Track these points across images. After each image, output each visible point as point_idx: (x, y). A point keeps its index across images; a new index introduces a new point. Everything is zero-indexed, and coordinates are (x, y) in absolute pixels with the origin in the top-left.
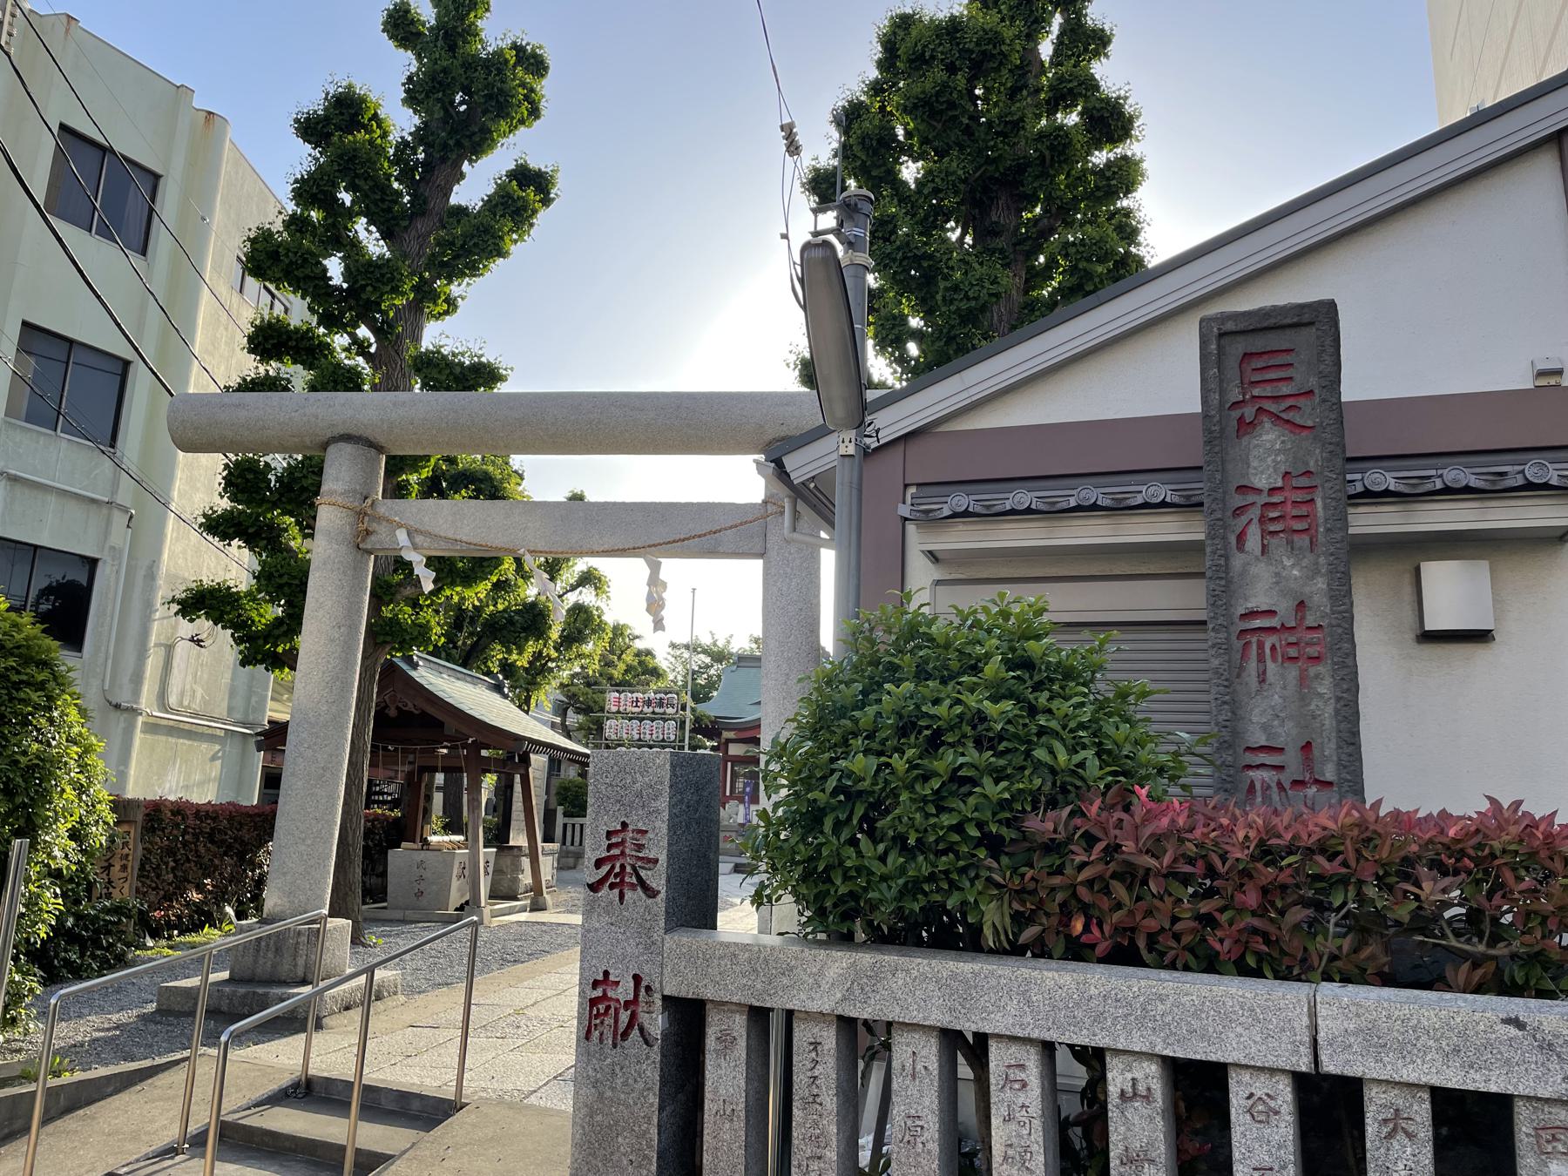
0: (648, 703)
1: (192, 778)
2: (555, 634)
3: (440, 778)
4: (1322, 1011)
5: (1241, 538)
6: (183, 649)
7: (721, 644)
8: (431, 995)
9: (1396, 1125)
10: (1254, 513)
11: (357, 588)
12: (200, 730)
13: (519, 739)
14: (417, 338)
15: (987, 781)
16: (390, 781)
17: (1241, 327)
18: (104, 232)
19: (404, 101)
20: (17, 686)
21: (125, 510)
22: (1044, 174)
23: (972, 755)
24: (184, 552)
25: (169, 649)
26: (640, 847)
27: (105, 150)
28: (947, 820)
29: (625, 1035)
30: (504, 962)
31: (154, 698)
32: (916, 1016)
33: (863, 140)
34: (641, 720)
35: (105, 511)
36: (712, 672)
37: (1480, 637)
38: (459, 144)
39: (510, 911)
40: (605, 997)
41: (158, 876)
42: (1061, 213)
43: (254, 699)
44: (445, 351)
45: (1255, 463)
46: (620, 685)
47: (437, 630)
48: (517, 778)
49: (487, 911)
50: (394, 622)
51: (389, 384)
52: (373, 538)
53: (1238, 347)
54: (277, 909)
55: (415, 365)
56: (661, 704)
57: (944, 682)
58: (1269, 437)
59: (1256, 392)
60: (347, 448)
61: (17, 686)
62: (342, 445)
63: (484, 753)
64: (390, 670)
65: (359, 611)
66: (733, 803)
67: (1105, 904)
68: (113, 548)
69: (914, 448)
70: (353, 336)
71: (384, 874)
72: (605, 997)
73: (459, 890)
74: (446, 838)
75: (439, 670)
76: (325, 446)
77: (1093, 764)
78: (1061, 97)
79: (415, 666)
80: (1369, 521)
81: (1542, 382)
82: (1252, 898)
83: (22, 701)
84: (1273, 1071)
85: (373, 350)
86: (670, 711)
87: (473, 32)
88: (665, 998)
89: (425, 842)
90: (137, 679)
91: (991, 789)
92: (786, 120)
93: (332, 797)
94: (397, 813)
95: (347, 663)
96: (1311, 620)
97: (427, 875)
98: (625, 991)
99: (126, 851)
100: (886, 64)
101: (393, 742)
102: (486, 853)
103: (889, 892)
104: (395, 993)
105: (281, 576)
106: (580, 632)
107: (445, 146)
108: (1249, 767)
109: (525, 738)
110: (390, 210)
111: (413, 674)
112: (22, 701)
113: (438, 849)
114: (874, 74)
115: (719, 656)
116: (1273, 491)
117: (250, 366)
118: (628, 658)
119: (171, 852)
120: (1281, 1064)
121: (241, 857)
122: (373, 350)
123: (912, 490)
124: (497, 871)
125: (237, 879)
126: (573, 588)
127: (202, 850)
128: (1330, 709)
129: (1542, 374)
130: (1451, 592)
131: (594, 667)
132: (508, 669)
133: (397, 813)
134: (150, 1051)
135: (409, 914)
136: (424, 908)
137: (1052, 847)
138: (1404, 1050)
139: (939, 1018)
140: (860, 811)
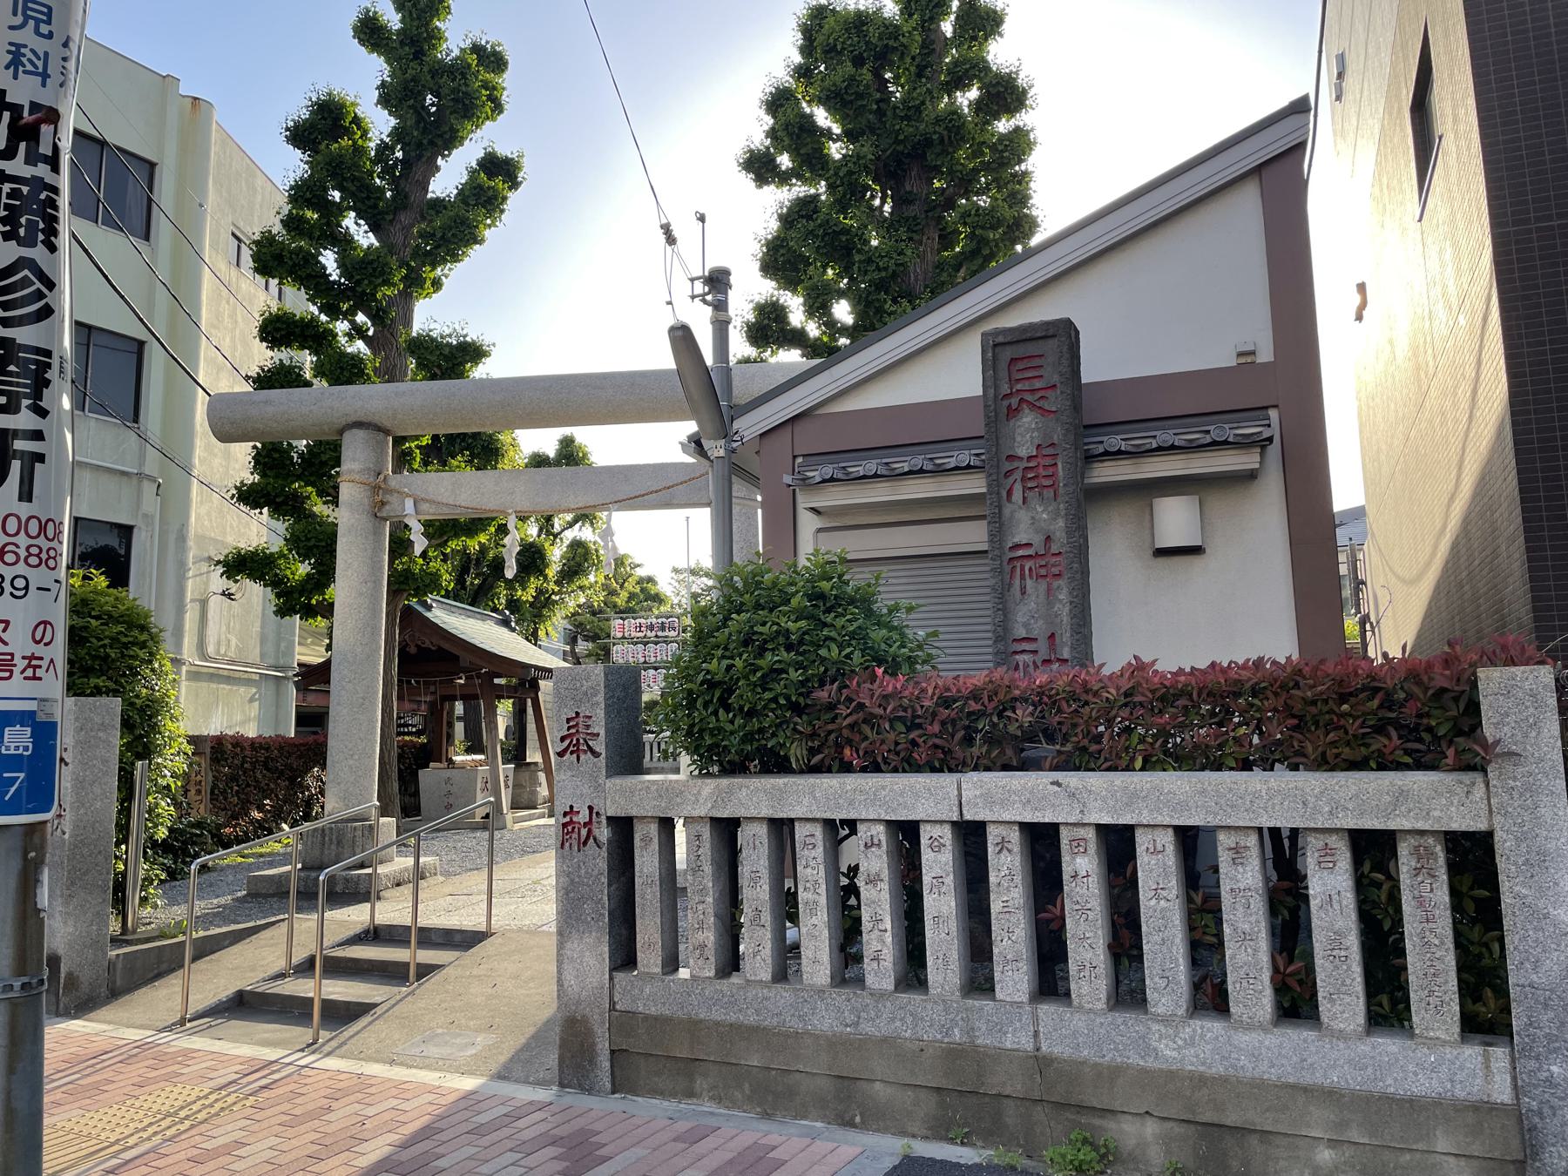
0: (651, 627)
1: (241, 716)
2: (552, 572)
3: (459, 708)
4: (964, 786)
5: (1010, 493)
6: (216, 602)
8: (465, 876)
9: (1002, 845)
10: (1018, 475)
11: (379, 549)
12: (237, 675)
13: (527, 667)
14: (408, 322)
15: (791, 670)
16: (414, 713)
17: (1008, 339)
18: (110, 223)
19: (379, 102)
20: (126, 646)
21: (153, 480)
22: (945, 152)
23: (784, 655)
24: (209, 514)
25: (204, 603)
26: (588, 727)
27: (102, 143)
28: (768, 695)
29: (585, 843)
30: (524, 853)
32: (753, 813)
33: (787, 126)
35: (135, 481)
37: (1195, 551)
38: (432, 143)
39: (530, 818)
40: (572, 821)
42: (966, 184)
43: (283, 645)
44: (434, 334)
45: (1018, 439)
47: (446, 576)
51: (390, 374)
53: (1007, 354)
55: (409, 347)
56: (663, 629)
57: (771, 611)
58: (1028, 419)
59: (1019, 387)
60: (360, 434)
61: (126, 646)
62: (355, 431)
63: (496, 681)
64: (408, 611)
65: (382, 567)
67: (857, 738)
68: (145, 516)
69: (799, 427)
70: (353, 323)
72: (572, 821)
74: (469, 758)
75: (450, 610)
76: (341, 432)
77: (857, 657)
78: (958, 81)
79: (429, 608)
80: (1107, 473)
81: (1242, 360)
82: (936, 728)
83: (131, 657)
84: (942, 822)
85: (370, 333)
86: (672, 633)
87: (435, 36)
88: (609, 818)
89: (450, 761)
91: (795, 675)
92: (664, 221)
93: (372, 721)
94: (423, 739)
95: (375, 612)
96: (1054, 549)
97: (454, 789)
98: (583, 817)
100: (807, 49)
101: (415, 675)
102: (505, 769)
103: (735, 740)
105: (308, 540)
107: (420, 145)
108: (1016, 653)
109: (532, 666)
110: (375, 206)
111: (428, 615)
112: (131, 657)
113: (462, 767)
114: (798, 59)
116: (1030, 458)
117: (262, 356)
118: (629, 586)
119: (233, 778)
120: (944, 818)
121: (292, 780)
122: (370, 333)
123: (800, 460)
125: (290, 800)
126: (571, 525)
128: (1067, 609)
129: (1240, 354)
130: (1175, 519)
131: (598, 599)
132: (514, 605)
133: (423, 739)
134: (249, 918)
137: (831, 707)
138: (1004, 803)
139: (766, 812)
140: (717, 694)
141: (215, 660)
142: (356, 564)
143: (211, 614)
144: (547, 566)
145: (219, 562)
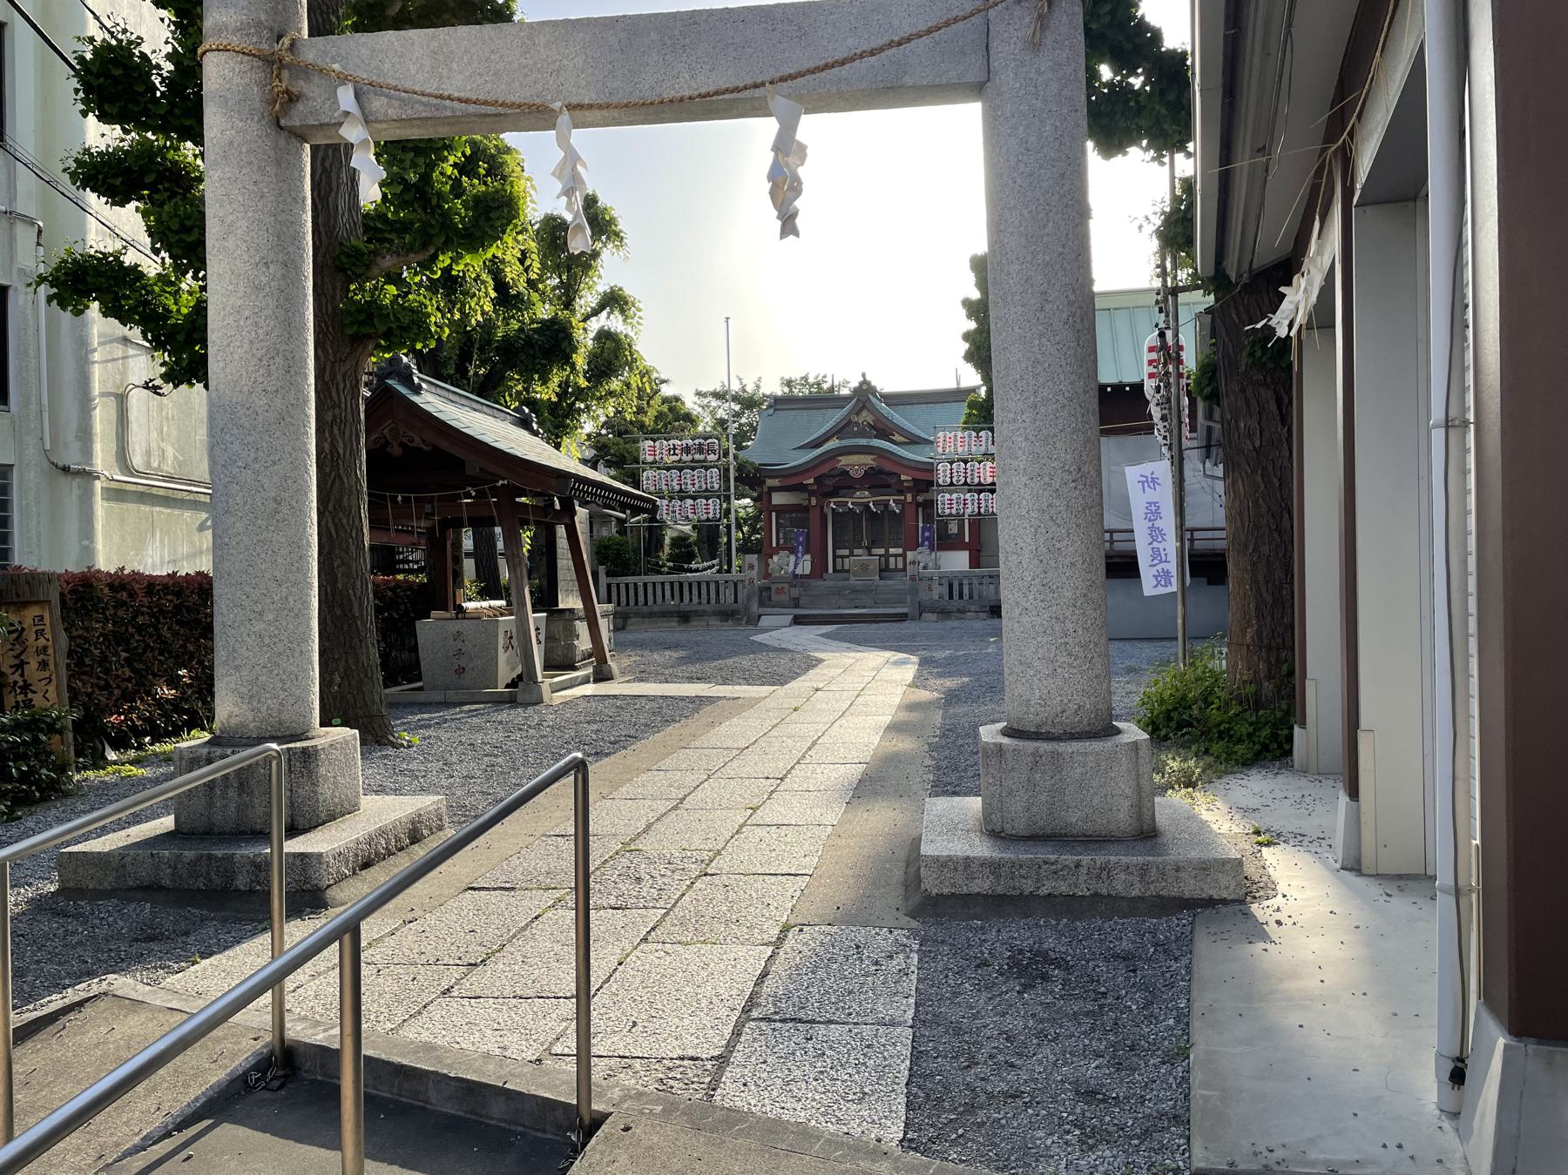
0: (687, 450)
2: (580, 360)
6: (138, 398)
7: (750, 389)
12: (179, 495)
21: (31, 222)
25: (122, 399)
31: (112, 459)
34: (680, 469)
36: (743, 420)
41: (107, 671)
46: (653, 434)
48: (561, 531)
49: (545, 688)
50: (372, 310)
52: (300, 106)
54: (234, 721)
56: (700, 450)
66: (783, 553)
71: (415, 649)
73: (508, 662)
74: (485, 604)
86: (712, 457)
89: (460, 609)
90: (85, 435)
93: (298, 546)
99: (42, 641)
102: (535, 619)
104: (440, 828)
106: (610, 363)
111: (415, 399)
113: (476, 617)
115: (749, 403)
119: (120, 639)
124: (550, 638)
126: (596, 312)
127: (165, 632)
133: (422, 578)
135: (452, 695)
136: (466, 688)
141: (146, 475)
142: (243, 223)
143: (133, 414)
144: (575, 350)
145: (42, 279)
